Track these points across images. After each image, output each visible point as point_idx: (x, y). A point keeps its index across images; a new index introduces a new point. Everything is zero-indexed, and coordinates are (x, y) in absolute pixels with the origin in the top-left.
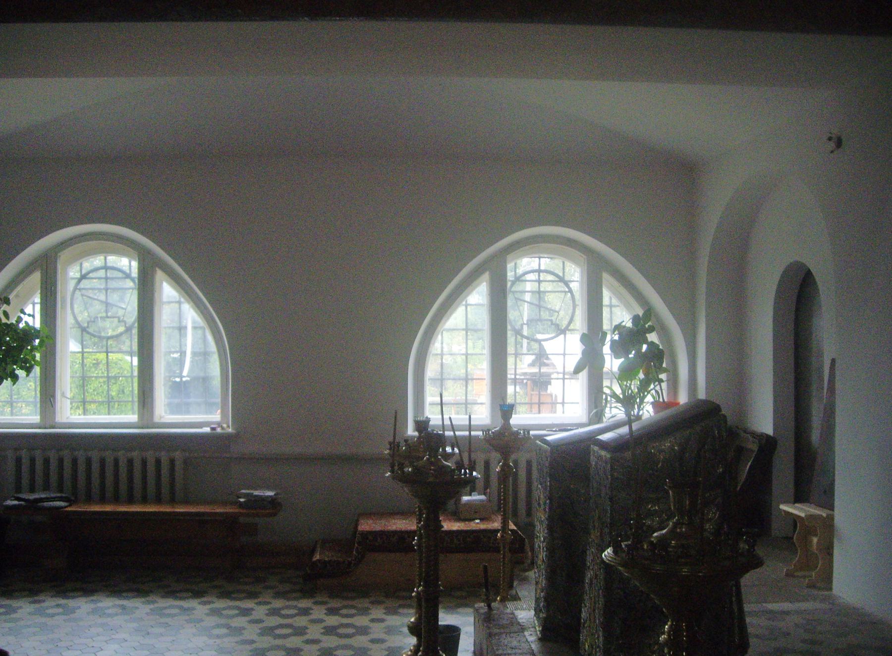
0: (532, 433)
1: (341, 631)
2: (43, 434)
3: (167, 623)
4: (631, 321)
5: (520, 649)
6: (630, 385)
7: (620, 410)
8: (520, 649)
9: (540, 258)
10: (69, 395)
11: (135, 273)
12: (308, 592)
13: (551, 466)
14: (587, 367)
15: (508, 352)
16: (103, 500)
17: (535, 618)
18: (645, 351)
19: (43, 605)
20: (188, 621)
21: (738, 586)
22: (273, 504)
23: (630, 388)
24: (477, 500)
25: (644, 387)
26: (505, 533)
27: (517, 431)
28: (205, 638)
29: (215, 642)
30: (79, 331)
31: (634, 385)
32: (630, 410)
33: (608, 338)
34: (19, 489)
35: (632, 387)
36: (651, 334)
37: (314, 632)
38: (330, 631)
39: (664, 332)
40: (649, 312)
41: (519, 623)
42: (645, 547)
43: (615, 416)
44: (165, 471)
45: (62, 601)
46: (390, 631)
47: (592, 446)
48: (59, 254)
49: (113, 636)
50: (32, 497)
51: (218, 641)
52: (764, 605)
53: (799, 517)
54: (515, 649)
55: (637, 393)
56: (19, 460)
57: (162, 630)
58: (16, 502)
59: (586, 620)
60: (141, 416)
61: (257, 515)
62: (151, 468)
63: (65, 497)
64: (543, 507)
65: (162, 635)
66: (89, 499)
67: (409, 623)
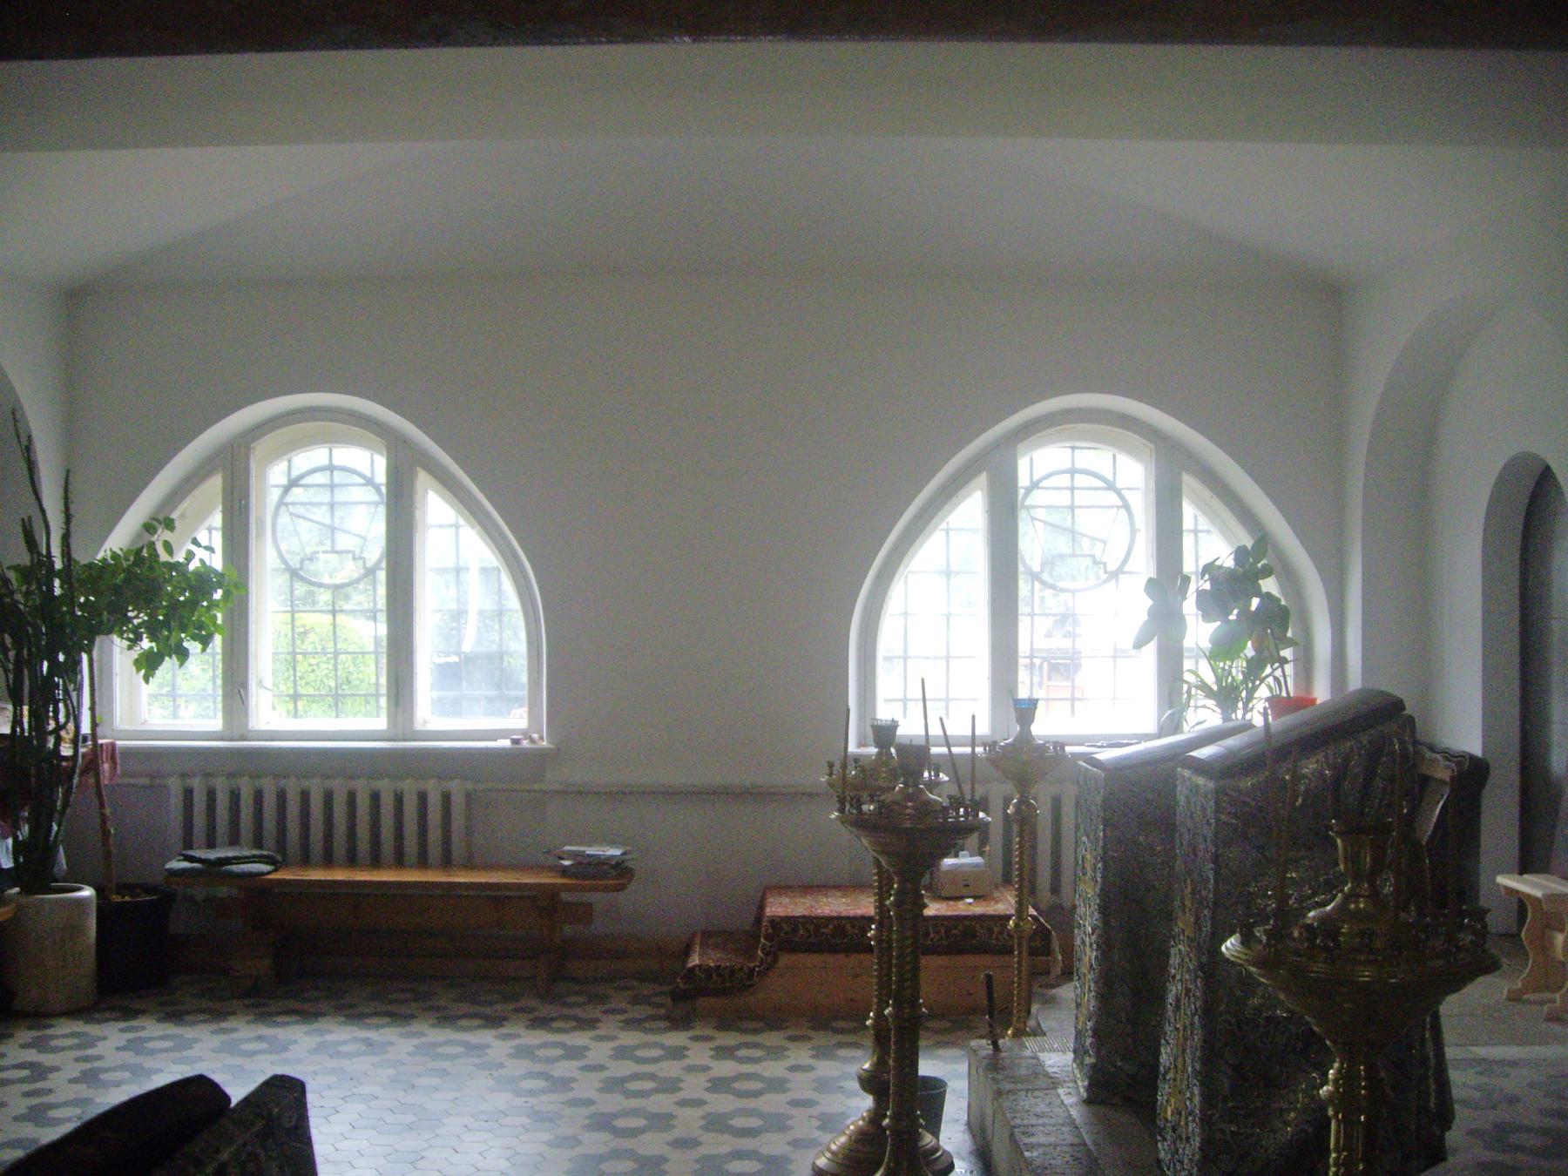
0: (1068, 749)
1: (742, 1086)
2: (228, 748)
3: (444, 1070)
4: (1233, 556)
5: (1051, 1118)
6: (1231, 667)
7: (1214, 711)
8: (1051, 1118)
9: (1073, 448)
10: (268, 682)
11: (381, 477)
12: (678, 1022)
13: (1107, 804)
14: (1156, 638)
15: (1020, 611)
16: (328, 861)
17: (1074, 1065)
18: (1257, 609)
19: (235, 1035)
20: (479, 1067)
21: (1436, 1017)
22: (619, 872)
23: (1230, 673)
24: (968, 865)
25: (1254, 670)
26: (1022, 919)
27: (1044, 744)
28: (508, 1096)
29: (526, 1102)
30: (287, 576)
31: (1237, 669)
32: (1230, 711)
33: (1192, 588)
34: (189, 845)
35: (1234, 671)
36: (1266, 580)
37: (694, 1086)
38: (718, 1085)
39: (1289, 576)
40: (1264, 541)
41: (1047, 1074)
42: (1296, 934)
43: (1202, 722)
44: (434, 816)
45: (264, 1030)
46: (823, 1086)
47: (1179, 769)
48: (253, 445)
49: (355, 1091)
50: (213, 855)
51: (532, 1101)
52: (1471, 1048)
53: (1529, 896)
54: (1042, 1117)
55: (1242, 683)
56: (188, 793)
57: (435, 1081)
58: (186, 865)
59: (1169, 1068)
60: (392, 718)
61: (596, 889)
62: (410, 808)
63: (267, 857)
64: (1089, 873)
65: (436, 1089)
66: (305, 861)
67: (862, 1071)
